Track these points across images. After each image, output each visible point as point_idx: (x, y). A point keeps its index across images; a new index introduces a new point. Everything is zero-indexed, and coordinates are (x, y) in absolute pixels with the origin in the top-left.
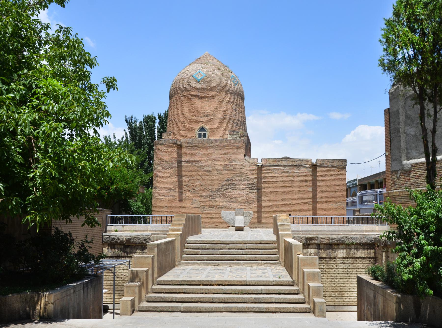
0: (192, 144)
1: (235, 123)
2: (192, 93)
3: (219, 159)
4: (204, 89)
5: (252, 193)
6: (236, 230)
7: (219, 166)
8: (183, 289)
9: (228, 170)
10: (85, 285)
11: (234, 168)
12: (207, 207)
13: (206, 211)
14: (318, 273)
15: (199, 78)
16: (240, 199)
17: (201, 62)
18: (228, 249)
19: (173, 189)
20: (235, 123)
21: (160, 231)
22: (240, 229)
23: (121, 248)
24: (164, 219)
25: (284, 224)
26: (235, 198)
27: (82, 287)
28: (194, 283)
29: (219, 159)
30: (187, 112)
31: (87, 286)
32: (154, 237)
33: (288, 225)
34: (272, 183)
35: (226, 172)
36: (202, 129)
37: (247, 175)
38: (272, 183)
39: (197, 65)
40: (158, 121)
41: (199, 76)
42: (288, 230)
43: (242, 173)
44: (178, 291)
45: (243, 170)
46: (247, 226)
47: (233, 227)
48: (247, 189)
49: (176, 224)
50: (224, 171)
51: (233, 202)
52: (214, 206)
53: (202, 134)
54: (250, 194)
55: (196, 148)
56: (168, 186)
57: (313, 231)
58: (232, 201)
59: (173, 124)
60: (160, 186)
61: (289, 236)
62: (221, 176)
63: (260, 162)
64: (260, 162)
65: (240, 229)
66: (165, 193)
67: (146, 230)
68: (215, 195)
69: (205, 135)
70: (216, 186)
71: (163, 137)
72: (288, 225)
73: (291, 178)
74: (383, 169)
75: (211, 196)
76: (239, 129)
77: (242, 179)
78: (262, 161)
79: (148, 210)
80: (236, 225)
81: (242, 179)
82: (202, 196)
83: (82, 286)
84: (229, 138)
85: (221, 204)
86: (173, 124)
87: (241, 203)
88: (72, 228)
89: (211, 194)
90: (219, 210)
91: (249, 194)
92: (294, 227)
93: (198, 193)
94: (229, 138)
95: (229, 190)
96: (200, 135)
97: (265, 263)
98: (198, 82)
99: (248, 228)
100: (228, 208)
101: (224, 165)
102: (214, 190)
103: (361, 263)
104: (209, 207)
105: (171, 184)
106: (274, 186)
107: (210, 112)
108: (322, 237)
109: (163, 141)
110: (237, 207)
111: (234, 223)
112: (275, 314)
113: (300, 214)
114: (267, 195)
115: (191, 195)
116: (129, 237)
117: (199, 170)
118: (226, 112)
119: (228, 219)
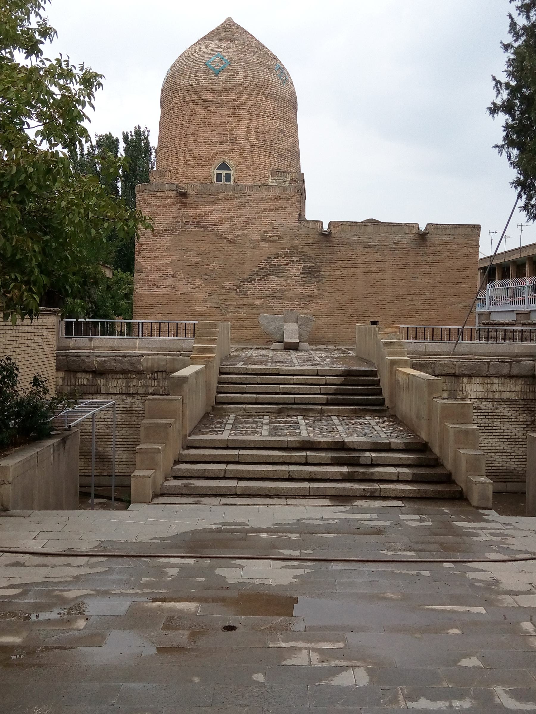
0: (205, 193)
1: (281, 156)
2: (203, 96)
3: (254, 221)
4: (225, 88)
5: (311, 283)
6: (285, 349)
7: (254, 236)
8: (210, 455)
9: (269, 241)
10: (56, 448)
11: (281, 238)
12: (231, 307)
13: (231, 314)
14: (474, 430)
15: (218, 68)
16: (290, 294)
17: (220, 38)
18: (294, 384)
19: (172, 273)
20: (281, 156)
21: (161, 349)
22: (292, 347)
23: (87, 379)
24: (164, 329)
25: (394, 342)
26: (280, 291)
27: (52, 452)
28: (252, 445)
29: (254, 221)
30: (196, 132)
31: (58, 450)
32: (147, 359)
33: (400, 344)
34: (347, 265)
35: (266, 244)
36: (224, 166)
37: (303, 250)
38: (347, 265)
39: (213, 42)
40: (122, 145)
41: (217, 65)
42: (401, 353)
43: (293, 247)
44: (226, 460)
45: (296, 242)
46: (304, 342)
47: (279, 342)
48: (303, 276)
49: (204, 339)
50: (263, 244)
51: (278, 298)
52: (244, 305)
53: (223, 175)
54: (309, 285)
55: (213, 200)
56: (163, 268)
57: (425, 353)
58: (275, 297)
59: (169, 153)
60: (149, 268)
61: (404, 363)
62: (257, 252)
63: (326, 227)
64: (326, 227)
65: (292, 347)
66: (159, 281)
67: (132, 348)
68: (247, 285)
69: (228, 178)
70: (249, 269)
71: (152, 179)
72: (400, 344)
73: (380, 259)
74: (309, 216)
75: (238, 287)
76: (289, 166)
77: (295, 259)
78: (329, 227)
79: (129, 313)
80: (286, 340)
81: (295, 259)
82: (224, 287)
83: (52, 450)
84: (270, 184)
85: (258, 302)
86: (169, 153)
87: (291, 300)
88: (9, 343)
89: (238, 283)
90: (254, 311)
91: (306, 285)
92: (412, 345)
93: (216, 282)
94: (271, 182)
95: (272, 277)
96: (219, 176)
97: (362, 410)
98: (217, 75)
99: (306, 346)
100: (269, 309)
101: (262, 231)
102: (245, 276)
103: (509, 409)
104: (236, 306)
105: (167, 265)
106: (351, 272)
107: (238, 134)
108: (443, 363)
109: (154, 187)
110: (283, 307)
111: (283, 336)
112: (251, 477)
113: (412, 323)
114: (338, 288)
115: (203, 285)
116: (103, 359)
117: (220, 241)
118: (267, 135)
119: (271, 328)
